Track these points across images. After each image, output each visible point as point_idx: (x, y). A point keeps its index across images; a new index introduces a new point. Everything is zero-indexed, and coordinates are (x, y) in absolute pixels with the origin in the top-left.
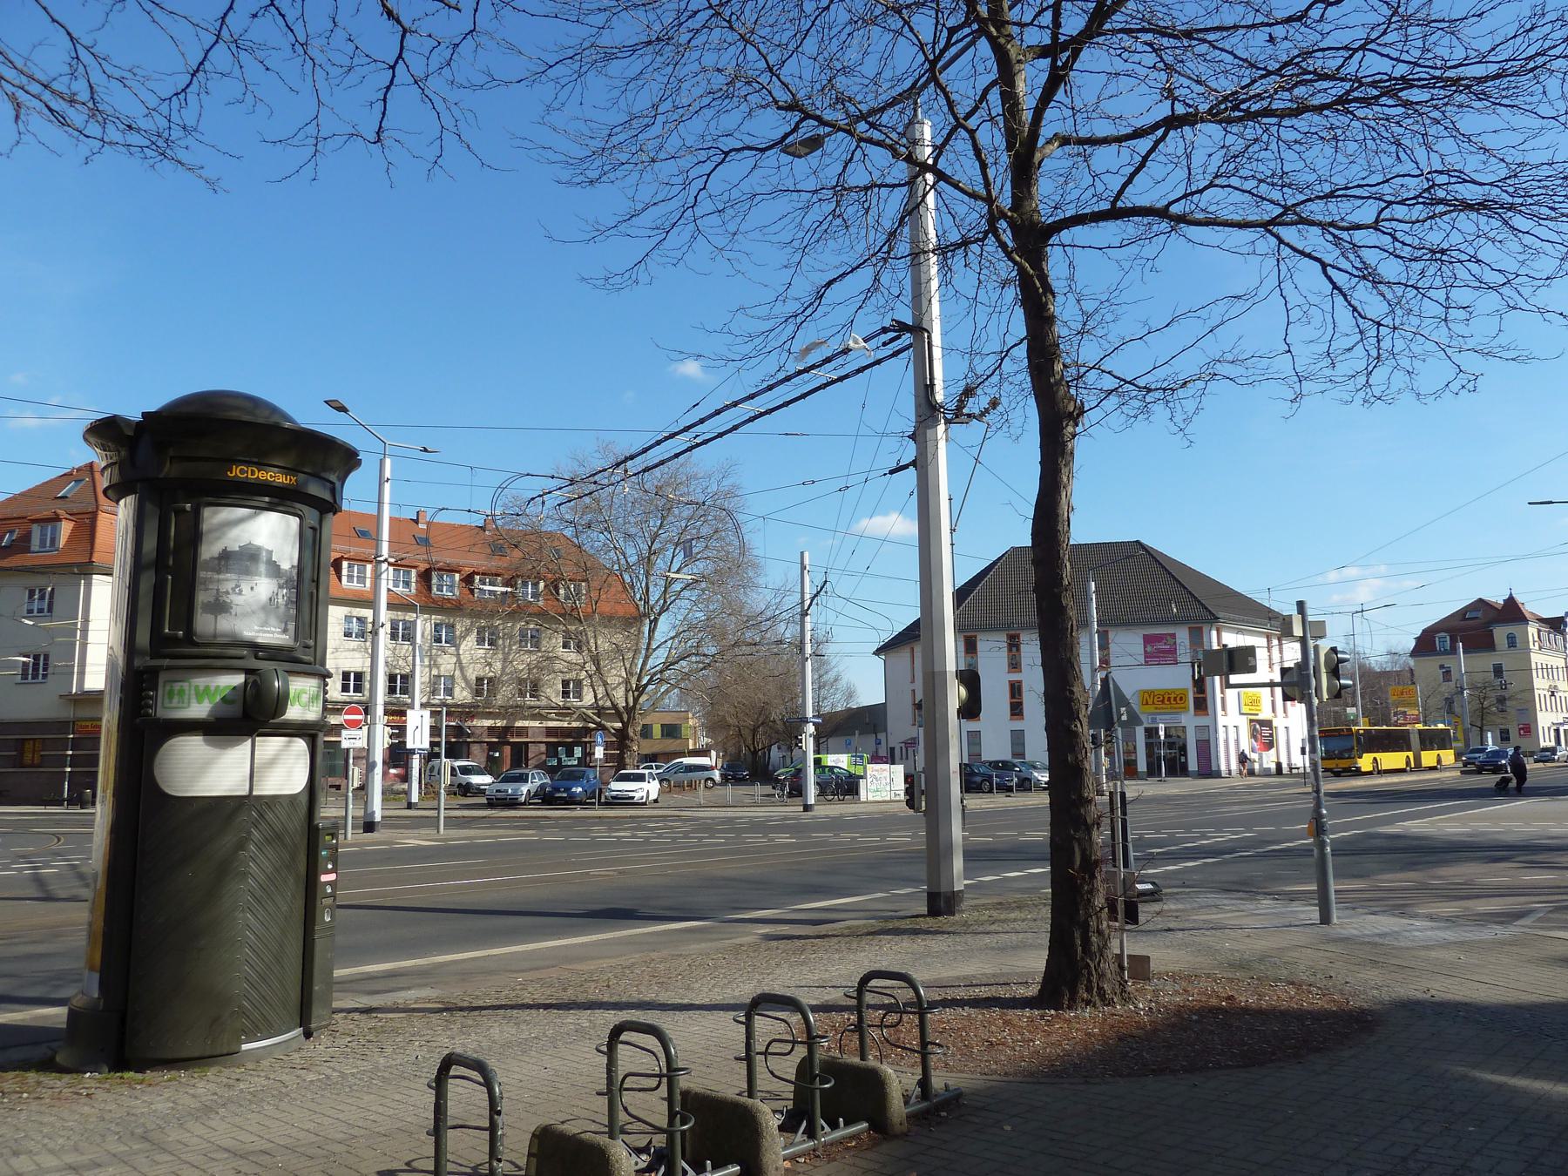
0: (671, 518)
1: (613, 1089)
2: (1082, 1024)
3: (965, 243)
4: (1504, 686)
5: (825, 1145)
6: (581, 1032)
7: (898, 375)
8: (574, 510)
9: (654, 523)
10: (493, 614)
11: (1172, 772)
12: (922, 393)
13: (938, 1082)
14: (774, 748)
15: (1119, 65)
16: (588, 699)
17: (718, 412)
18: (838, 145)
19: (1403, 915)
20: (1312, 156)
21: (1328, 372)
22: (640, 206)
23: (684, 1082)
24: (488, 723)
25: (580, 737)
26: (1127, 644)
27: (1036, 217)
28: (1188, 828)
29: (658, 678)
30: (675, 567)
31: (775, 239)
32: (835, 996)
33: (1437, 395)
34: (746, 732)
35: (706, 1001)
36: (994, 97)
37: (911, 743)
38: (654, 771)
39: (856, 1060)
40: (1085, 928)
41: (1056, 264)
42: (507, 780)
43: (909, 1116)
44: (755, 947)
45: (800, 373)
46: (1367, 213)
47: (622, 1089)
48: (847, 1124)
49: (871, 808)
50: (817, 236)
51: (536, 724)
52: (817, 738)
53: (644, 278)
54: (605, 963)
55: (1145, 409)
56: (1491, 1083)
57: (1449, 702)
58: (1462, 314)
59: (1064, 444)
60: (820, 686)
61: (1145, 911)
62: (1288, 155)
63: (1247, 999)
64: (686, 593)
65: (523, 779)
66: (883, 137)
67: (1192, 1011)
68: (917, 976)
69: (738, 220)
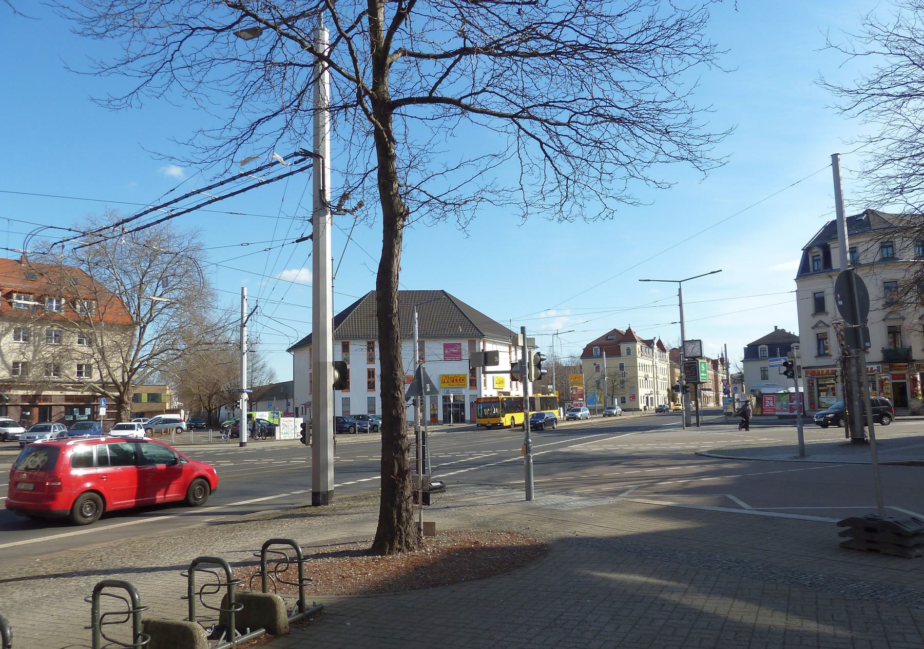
0: (156, 262)
1: (96, 623)
2: (397, 562)
3: (345, 107)
4: (624, 375)
5: (238, 644)
6: (79, 590)
7: (303, 183)
8: (88, 253)
9: (144, 265)
10: (26, 320)
11: (456, 421)
12: (318, 195)
13: (308, 602)
14: (223, 408)
15: (435, 12)
16: (96, 376)
17: (187, 196)
18: (269, 36)
19: (567, 494)
20: (542, 82)
21: (541, 202)
22: (132, 56)
23: (144, 615)
24: (21, 393)
25: (90, 402)
26: (435, 348)
27: (386, 95)
28: (463, 451)
29: (146, 363)
30: (158, 293)
31: (224, 88)
32: (249, 556)
33: (594, 219)
34: (205, 398)
35: (168, 565)
36: (365, 20)
37: (307, 405)
38: (142, 423)
39: (260, 593)
40: (399, 508)
41: (397, 125)
42: (36, 430)
43: (290, 623)
44: (202, 530)
45: (241, 175)
46: (564, 116)
47: (101, 623)
48: (251, 631)
49: (281, 444)
50: (253, 90)
51: (58, 393)
52: (250, 402)
53: (135, 103)
54: (99, 546)
55: (444, 215)
56: (600, 577)
57: (598, 383)
58: (608, 177)
59: (397, 231)
60: (252, 370)
61: (433, 497)
62: (526, 79)
63: (485, 542)
64: (166, 310)
65: (47, 429)
66: (295, 34)
67: (456, 551)
68: (300, 542)
69: (202, 73)
